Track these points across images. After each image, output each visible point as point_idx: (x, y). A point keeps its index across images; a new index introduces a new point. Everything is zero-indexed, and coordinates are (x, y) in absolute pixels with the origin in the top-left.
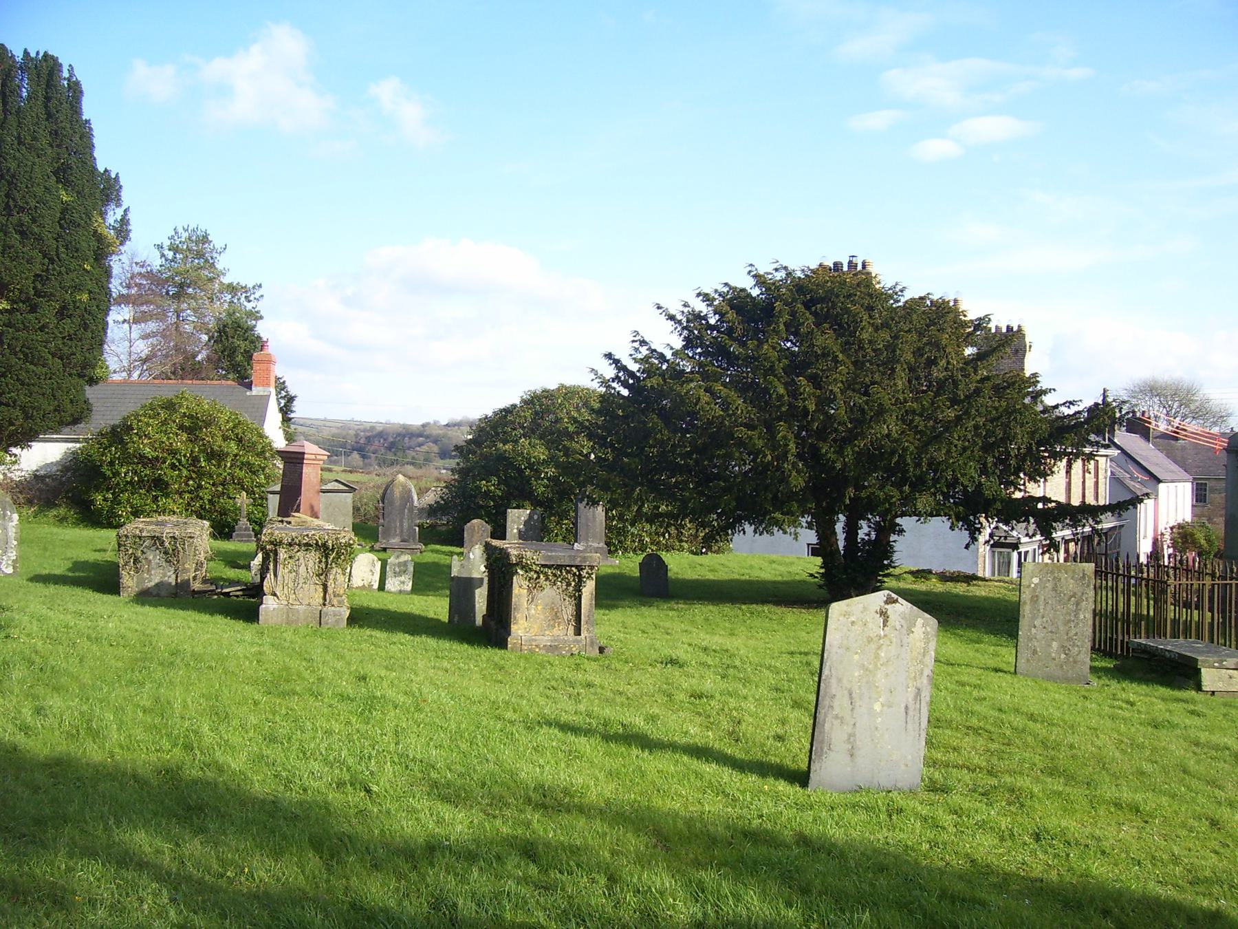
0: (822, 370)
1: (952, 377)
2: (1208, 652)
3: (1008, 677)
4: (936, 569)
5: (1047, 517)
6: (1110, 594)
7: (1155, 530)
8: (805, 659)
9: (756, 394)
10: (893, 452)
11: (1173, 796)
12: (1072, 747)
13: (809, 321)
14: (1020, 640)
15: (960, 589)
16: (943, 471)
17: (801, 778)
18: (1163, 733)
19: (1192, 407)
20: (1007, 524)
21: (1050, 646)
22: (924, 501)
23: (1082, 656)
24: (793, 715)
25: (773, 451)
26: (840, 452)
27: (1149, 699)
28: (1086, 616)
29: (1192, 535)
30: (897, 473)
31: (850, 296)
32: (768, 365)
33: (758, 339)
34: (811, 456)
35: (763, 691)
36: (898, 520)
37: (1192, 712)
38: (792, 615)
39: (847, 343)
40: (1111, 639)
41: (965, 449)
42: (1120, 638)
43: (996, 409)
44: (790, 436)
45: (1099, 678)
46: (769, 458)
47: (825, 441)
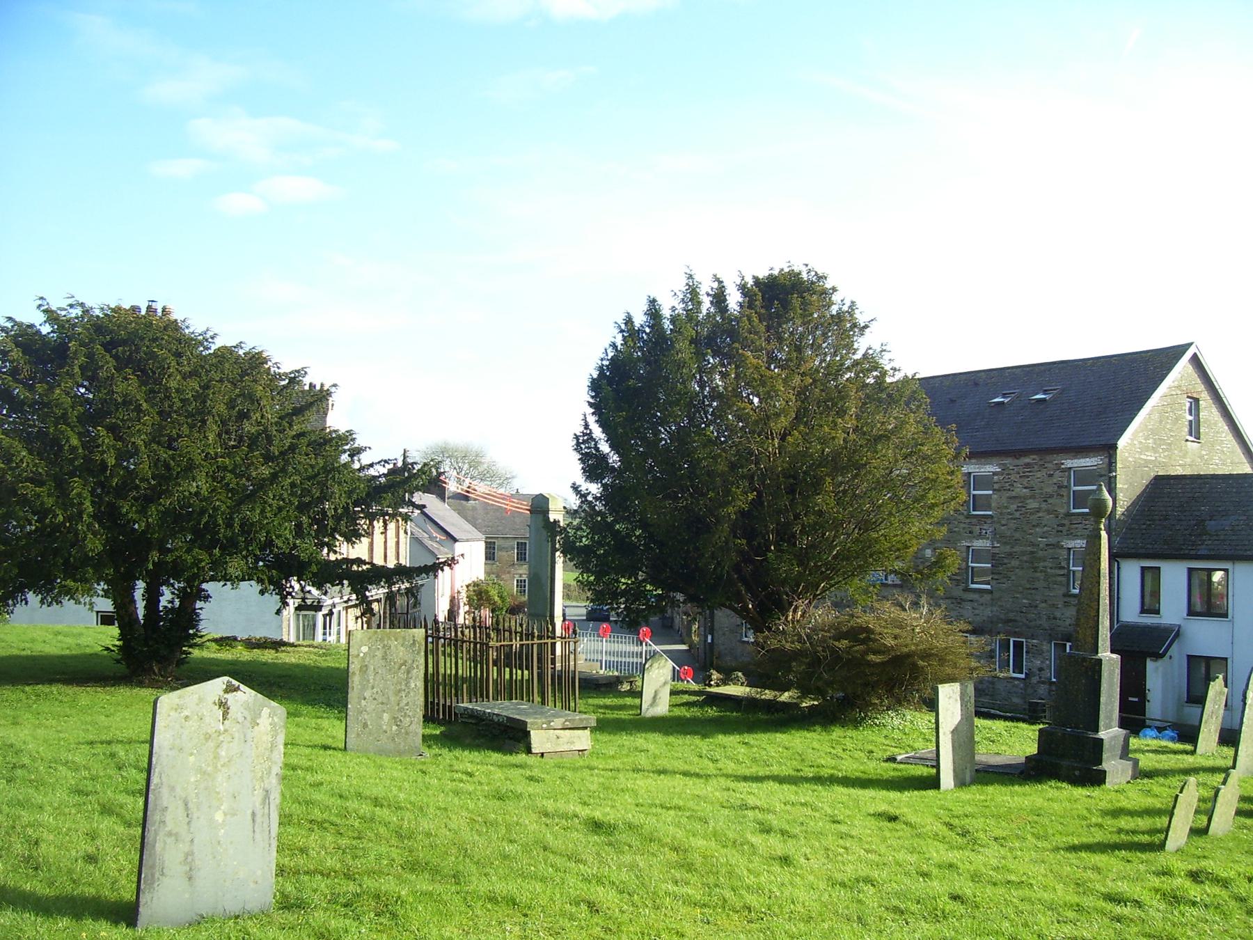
0: (122, 420)
1: (265, 431)
2: (535, 713)
3: (339, 754)
4: (242, 635)
5: (361, 578)
6: (448, 659)
7: (452, 588)
8: (109, 749)
9: (47, 446)
10: (203, 512)
11: (543, 880)
12: (428, 835)
13: (108, 365)
14: (350, 713)
15: (268, 656)
16: (256, 532)
17: (127, 914)
18: (510, 805)
19: (481, 469)
20: (319, 586)
21: (381, 718)
22: (235, 565)
23: (413, 727)
24: (106, 824)
25: (65, 510)
26: (143, 511)
27: (484, 766)
28: (418, 684)
29: (487, 592)
30: (205, 537)
31: (155, 340)
32: (59, 412)
33: (48, 383)
34: (109, 516)
35: (61, 794)
36: (204, 586)
37: (531, 779)
38: (87, 696)
39: (152, 391)
40: (432, 703)
41: (280, 509)
42: (442, 702)
43: (312, 467)
44: (86, 494)
45: (429, 747)
46: (61, 518)
47: (125, 499)
